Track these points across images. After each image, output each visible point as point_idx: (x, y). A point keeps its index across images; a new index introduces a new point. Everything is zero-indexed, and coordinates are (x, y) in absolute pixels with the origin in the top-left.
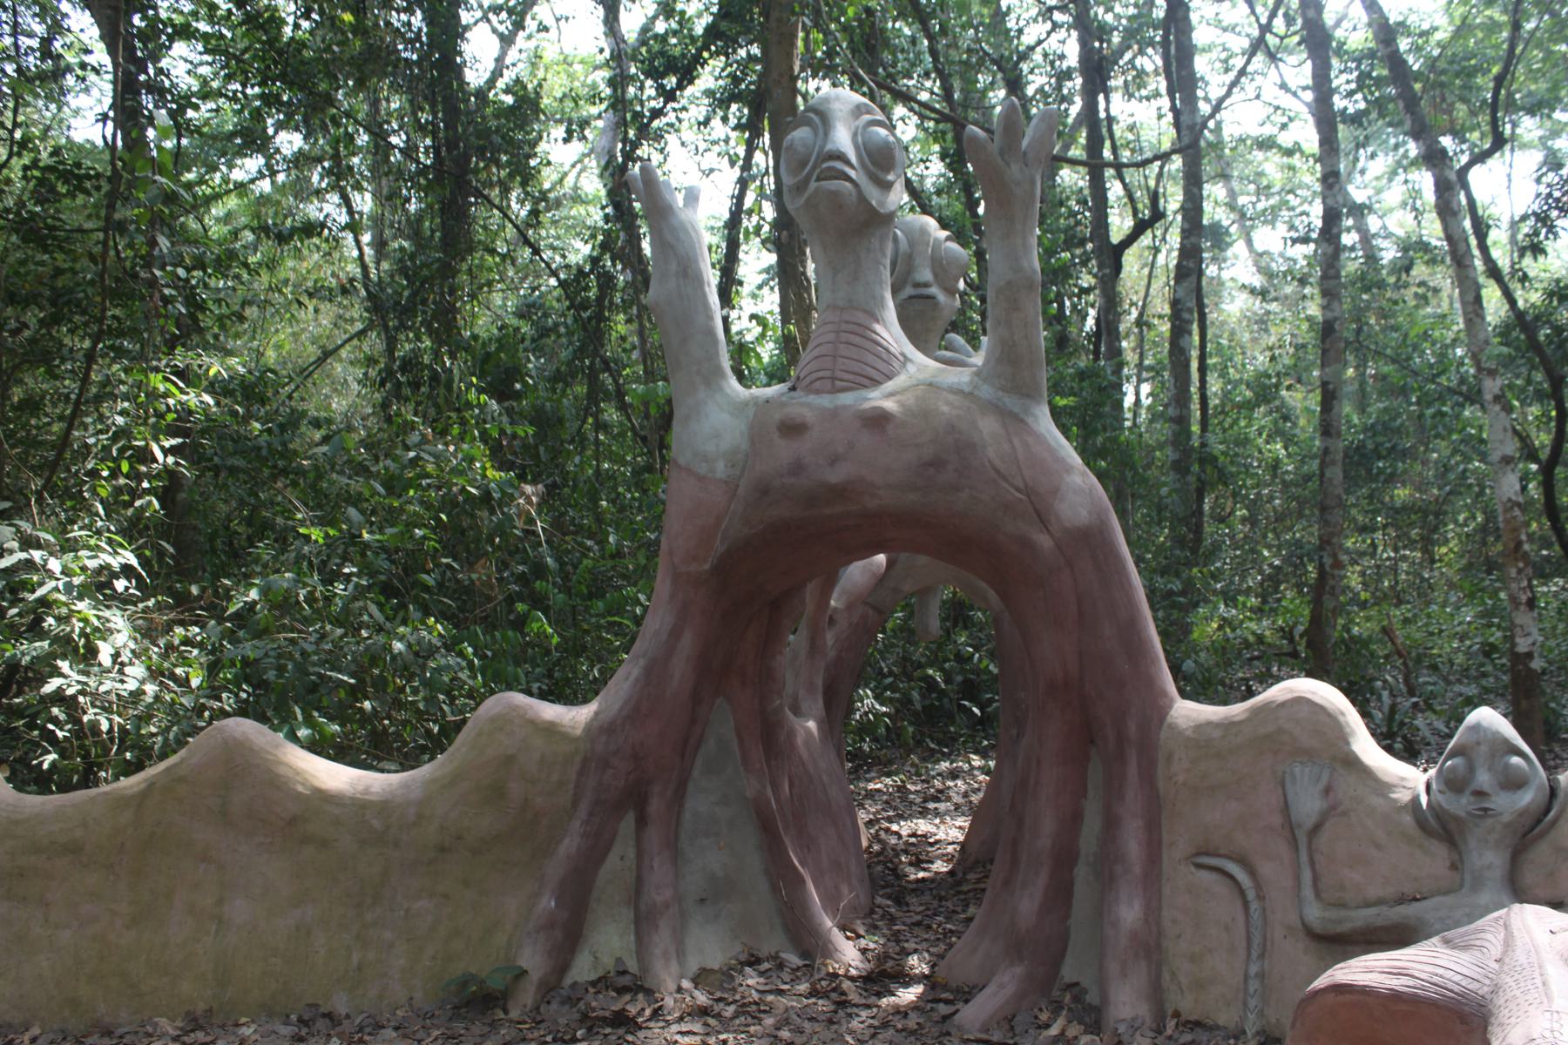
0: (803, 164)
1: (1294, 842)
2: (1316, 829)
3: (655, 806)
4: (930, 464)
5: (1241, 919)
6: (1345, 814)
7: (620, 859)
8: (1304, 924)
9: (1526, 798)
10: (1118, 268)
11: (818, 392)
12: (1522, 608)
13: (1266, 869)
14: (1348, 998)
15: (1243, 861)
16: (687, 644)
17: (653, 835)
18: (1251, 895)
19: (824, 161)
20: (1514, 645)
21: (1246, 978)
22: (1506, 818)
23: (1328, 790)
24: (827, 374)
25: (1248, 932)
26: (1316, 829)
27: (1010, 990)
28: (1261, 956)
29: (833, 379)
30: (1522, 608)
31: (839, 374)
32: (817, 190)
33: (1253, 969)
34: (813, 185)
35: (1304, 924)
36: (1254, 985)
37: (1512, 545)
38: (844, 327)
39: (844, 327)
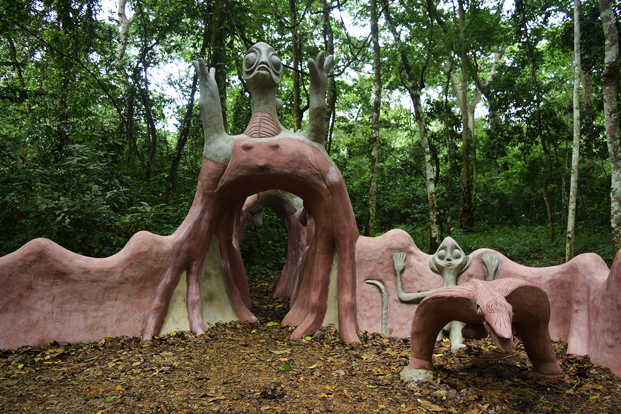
0: (252, 65)
1: (396, 275)
2: (402, 271)
3: (194, 269)
4: (292, 161)
5: (380, 298)
6: (411, 266)
7: (182, 286)
8: (399, 298)
9: (460, 261)
10: (302, 116)
11: (254, 137)
12: (434, 224)
13: (388, 283)
14: (437, 300)
15: (381, 281)
16: (206, 215)
17: (193, 278)
18: (383, 291)
19: (261, 64)
20: (431, 235)
21: (382, 314)
22: (456, 266)
23: (405, 260)
24: (258, 132)
25: (382, 301)
26: (402, 271)
27: (311, 322)
28: (387, 308)
29: (259, 133)
30: (434, 224)
31: (261, 132)
32: (258, 73)
33: (384, 312)
34: (256, 72)
35: (399, 298)
36: (384, 316)
37: (432, 205)
38: (263, 117)
39: (263, 117)
